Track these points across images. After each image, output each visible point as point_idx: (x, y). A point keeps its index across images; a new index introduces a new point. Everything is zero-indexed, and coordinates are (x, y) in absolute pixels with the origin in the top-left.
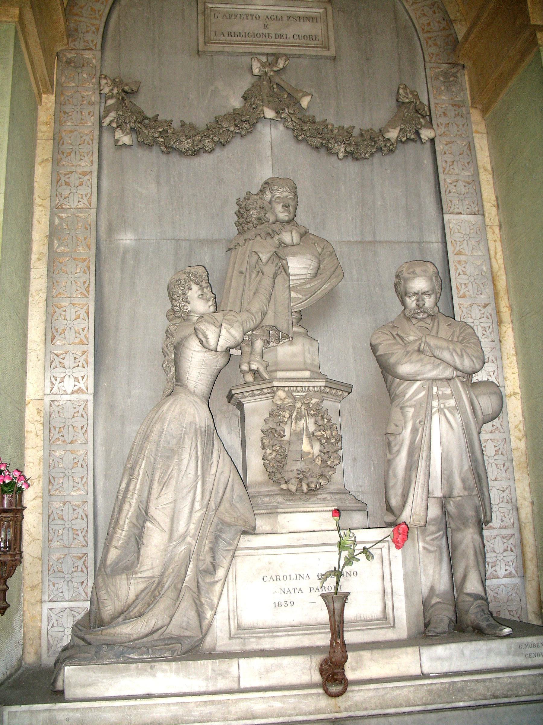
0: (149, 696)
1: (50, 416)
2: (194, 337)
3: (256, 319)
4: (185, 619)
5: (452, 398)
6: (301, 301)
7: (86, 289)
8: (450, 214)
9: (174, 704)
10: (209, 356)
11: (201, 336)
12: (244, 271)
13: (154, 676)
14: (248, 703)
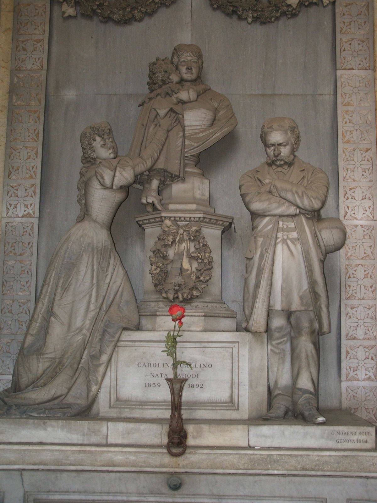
0: (41, 444)
1: (6, 234)
2: (95, 178)
3: (146, 163)
4: (79, 391)
5: (295, 231)
6: (193, 147)
7: (36, 135)
8: (343, 69)
9: (56, 450)
10: (107, 193)
11: (99, 177)
12: (145, 124)
13: (46, 429)
14: (110, 455)
